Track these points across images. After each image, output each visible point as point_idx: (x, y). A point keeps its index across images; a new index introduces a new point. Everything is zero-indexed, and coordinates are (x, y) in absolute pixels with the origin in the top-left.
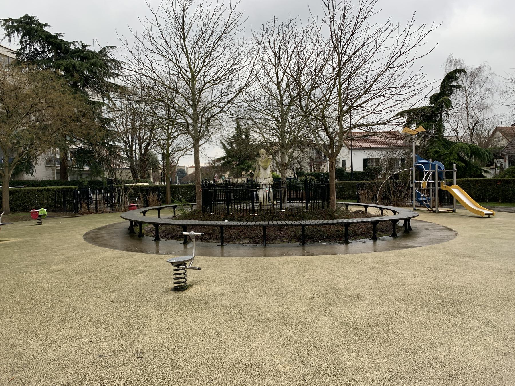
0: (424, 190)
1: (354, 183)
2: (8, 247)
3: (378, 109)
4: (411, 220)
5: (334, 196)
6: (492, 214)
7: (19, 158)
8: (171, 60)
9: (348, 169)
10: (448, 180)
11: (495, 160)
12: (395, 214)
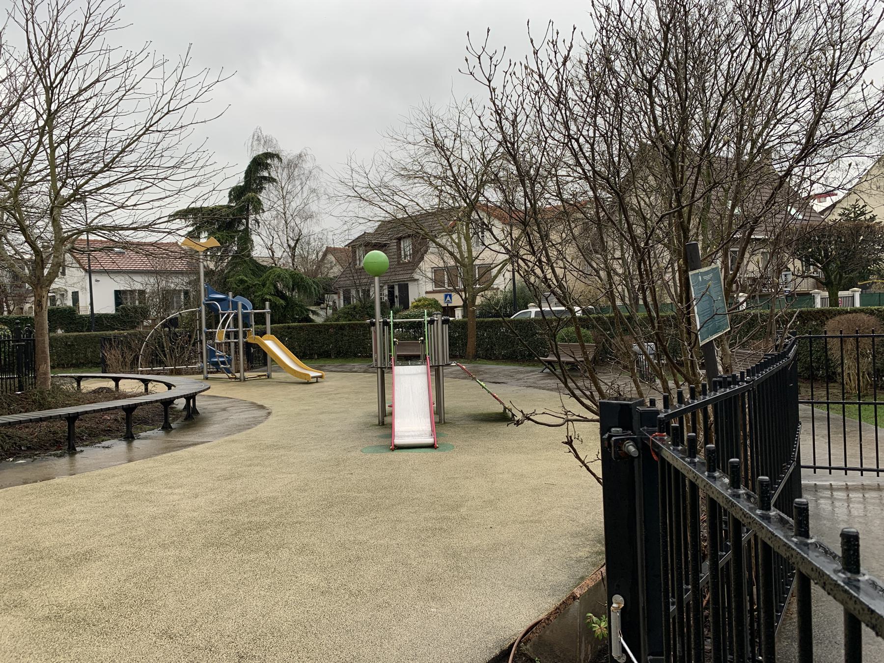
0: (219, 345)
1: (96, 336)
3: (130, 203)
4: (197, 398)
5: (46, 363)
6: (321, 377)
9: (84, 309)
10: (260, 326)
11: (326, 295)
12: (170, 388)
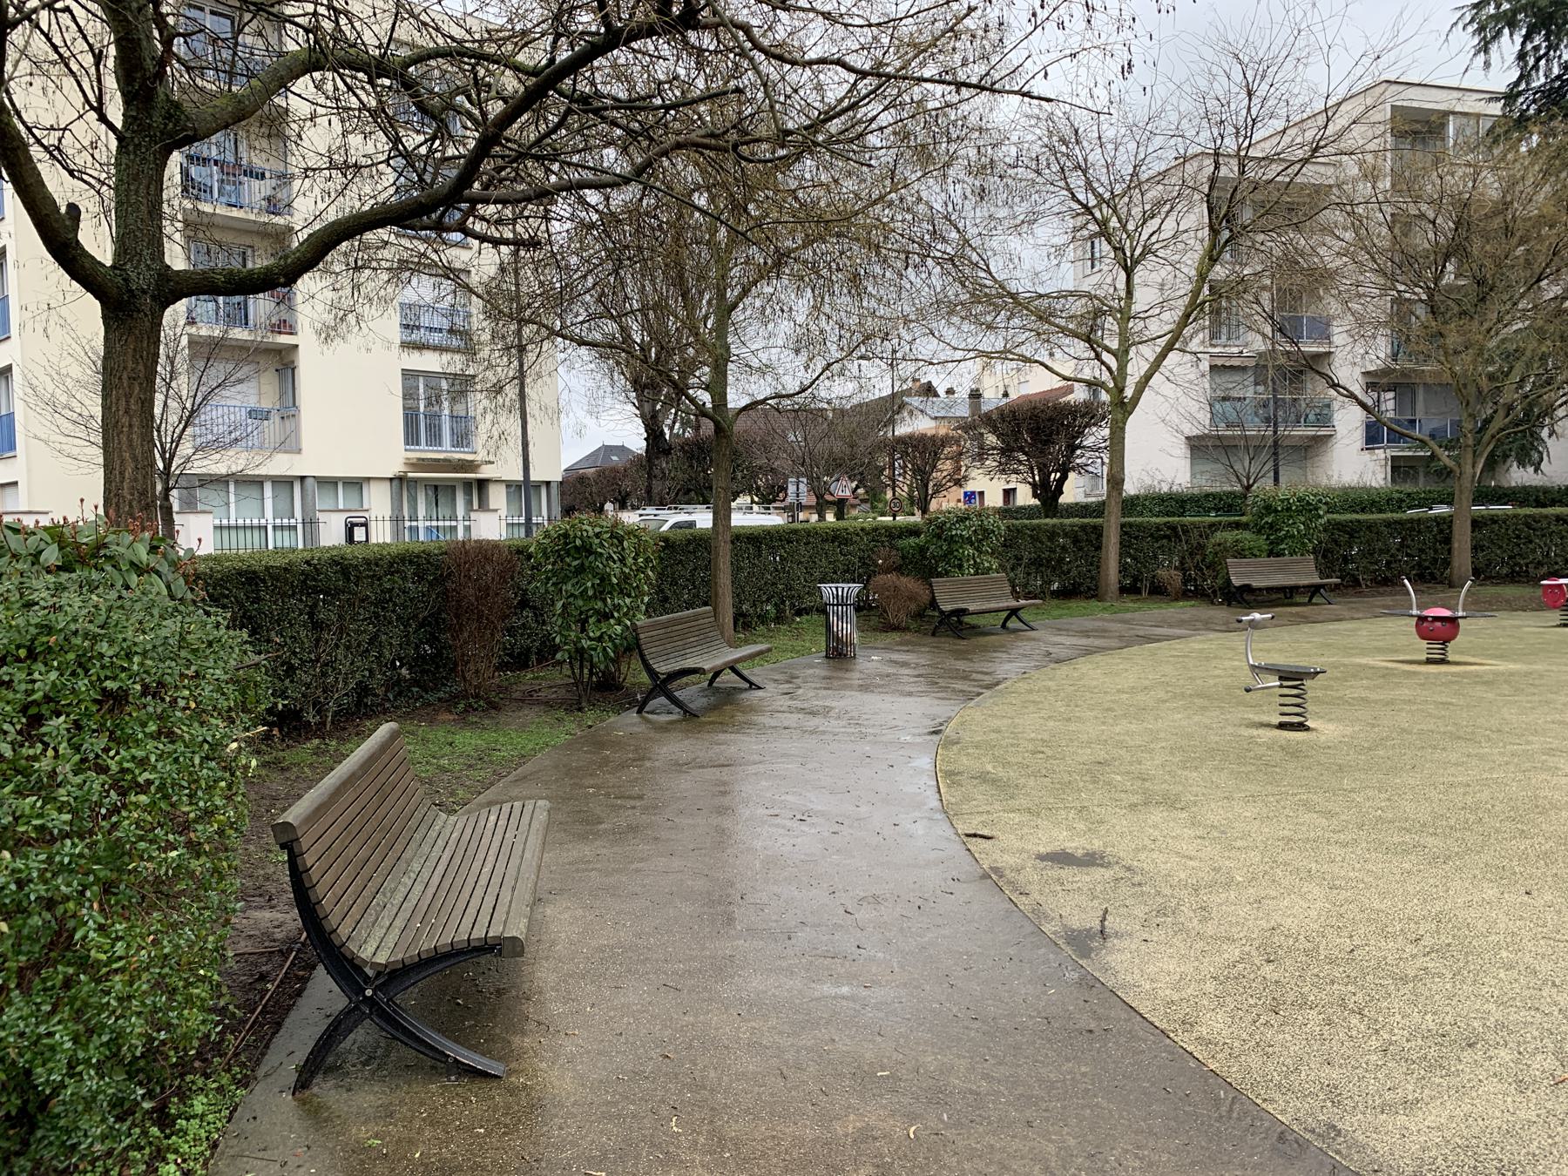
2: (1485, 683)
7: (1507, 420)
8: (42, 32)
